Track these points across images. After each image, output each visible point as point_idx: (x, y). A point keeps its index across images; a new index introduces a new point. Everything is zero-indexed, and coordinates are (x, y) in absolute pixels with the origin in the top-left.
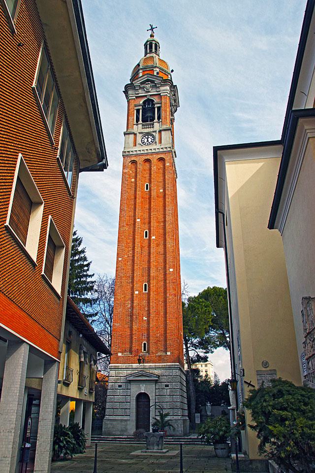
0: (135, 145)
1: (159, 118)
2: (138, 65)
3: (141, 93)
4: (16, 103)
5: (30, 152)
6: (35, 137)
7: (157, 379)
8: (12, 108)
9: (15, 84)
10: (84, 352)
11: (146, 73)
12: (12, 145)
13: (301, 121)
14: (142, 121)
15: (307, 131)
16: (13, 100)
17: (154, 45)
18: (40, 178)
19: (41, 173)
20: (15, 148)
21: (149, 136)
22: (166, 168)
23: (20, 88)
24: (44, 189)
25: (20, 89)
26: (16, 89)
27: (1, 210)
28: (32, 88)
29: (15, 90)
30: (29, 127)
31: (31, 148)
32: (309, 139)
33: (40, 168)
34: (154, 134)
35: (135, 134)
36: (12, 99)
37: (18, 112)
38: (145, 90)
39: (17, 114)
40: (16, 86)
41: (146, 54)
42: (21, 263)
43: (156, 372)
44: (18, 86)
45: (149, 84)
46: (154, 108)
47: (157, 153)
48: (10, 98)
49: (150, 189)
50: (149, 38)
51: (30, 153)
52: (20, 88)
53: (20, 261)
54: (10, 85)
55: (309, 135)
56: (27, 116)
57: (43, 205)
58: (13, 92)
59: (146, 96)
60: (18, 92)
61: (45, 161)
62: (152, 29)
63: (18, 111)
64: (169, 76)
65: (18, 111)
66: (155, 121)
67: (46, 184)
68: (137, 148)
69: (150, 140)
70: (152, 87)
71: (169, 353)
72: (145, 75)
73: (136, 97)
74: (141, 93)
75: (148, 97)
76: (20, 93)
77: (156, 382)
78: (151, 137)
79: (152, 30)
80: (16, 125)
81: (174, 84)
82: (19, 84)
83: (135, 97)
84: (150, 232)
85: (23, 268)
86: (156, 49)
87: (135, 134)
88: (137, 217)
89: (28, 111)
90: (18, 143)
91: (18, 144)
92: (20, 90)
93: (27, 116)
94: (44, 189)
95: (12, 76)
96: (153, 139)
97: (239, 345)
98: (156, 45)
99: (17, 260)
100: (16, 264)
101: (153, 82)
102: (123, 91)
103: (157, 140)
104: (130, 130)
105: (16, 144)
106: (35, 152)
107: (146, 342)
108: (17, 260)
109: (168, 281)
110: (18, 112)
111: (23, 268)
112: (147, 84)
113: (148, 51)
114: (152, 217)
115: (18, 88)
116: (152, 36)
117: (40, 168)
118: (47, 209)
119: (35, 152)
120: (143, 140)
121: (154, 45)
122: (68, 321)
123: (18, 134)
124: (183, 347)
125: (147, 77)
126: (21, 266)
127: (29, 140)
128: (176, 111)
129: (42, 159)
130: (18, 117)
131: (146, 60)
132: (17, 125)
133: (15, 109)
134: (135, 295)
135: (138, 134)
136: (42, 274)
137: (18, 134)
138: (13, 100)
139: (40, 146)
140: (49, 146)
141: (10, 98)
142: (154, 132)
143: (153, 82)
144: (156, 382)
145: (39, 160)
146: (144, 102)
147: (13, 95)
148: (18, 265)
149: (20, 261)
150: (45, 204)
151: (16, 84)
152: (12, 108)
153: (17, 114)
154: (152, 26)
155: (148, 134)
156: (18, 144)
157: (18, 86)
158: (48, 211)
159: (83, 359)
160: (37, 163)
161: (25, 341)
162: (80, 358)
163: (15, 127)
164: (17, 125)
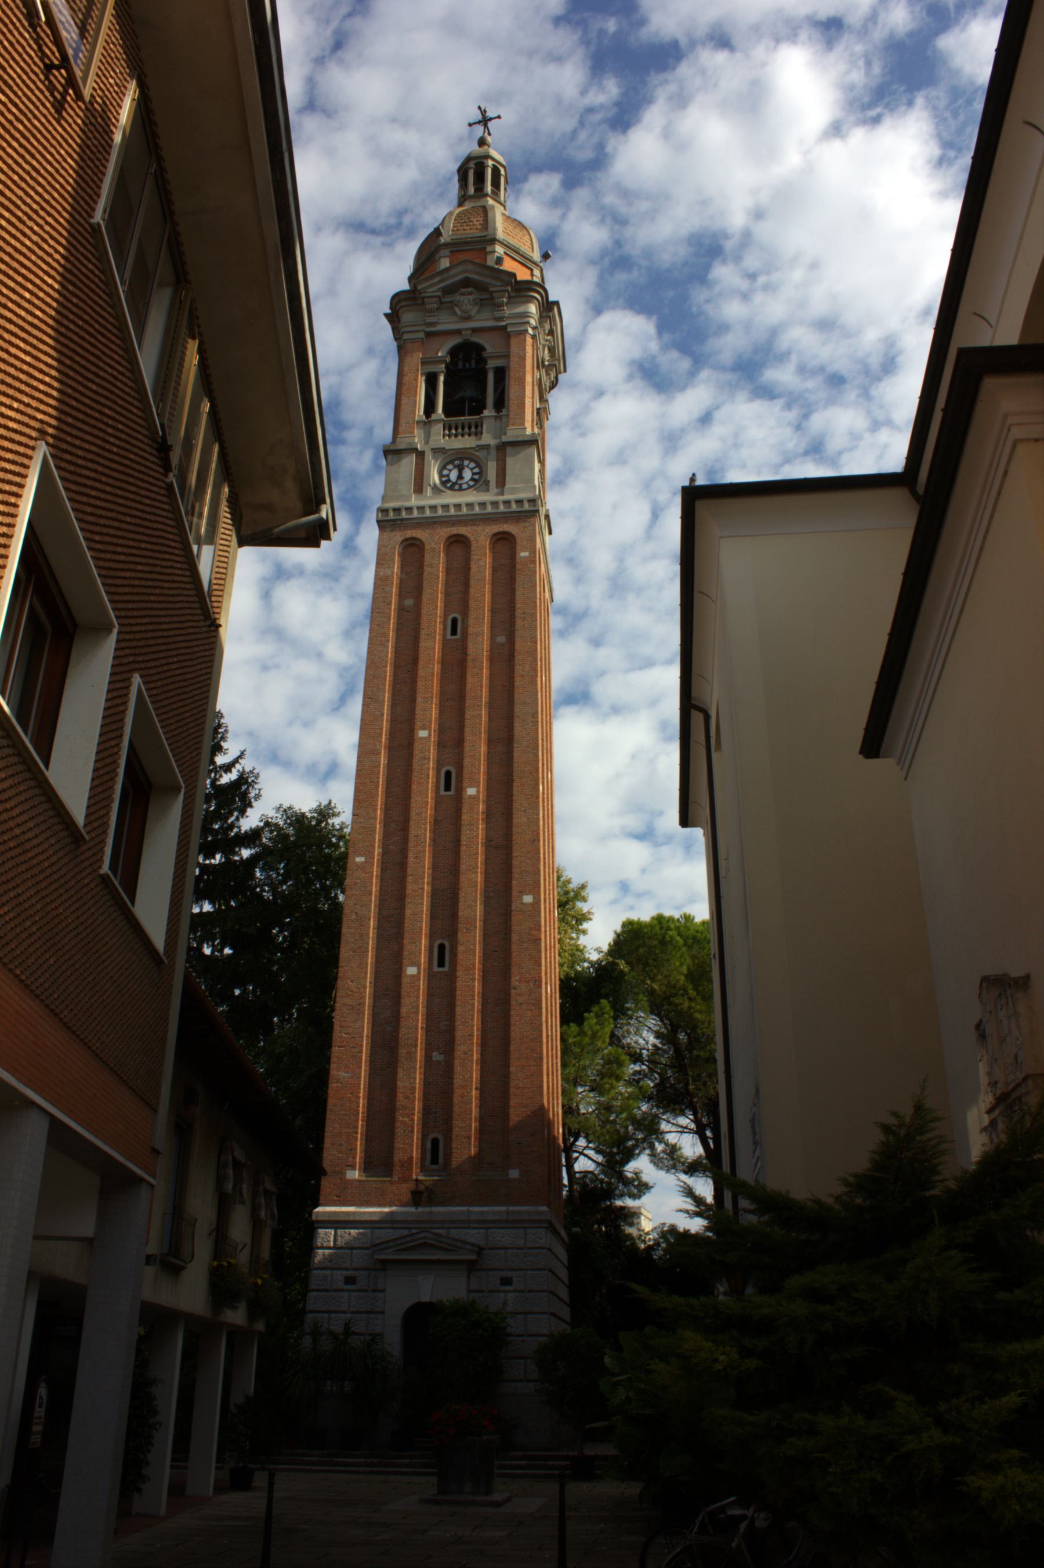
0: (419, 489)
2: (437, 233)
3: (446, 322)
4: (35, 264)
5: (77, 442)
6: (94, 396)
7: (473, 1257)
8: (20, 279)
9: (31, 197)
10: (236, 1164)
11: (462, 257)
12: (16, 405)
13: (990, 384)
14: (445, 411)
15: (1010, 421)
16: (24, 250)
17: (489, 172)
18: (108, 539)
19: (112, 523)
20: (26, 420)
21: (466, 463)
22: (518, 566)
23: (49, 214)
24: (119, 582)
25: (50, 220)
26: (35, 216)
27: (2, 848)
28: (91, 225)
29: (30, 218)
30: (77, 358)
31: (80, 429)
32: (1015, 443)
33: (109, 505)
34: (481, 454)
35: (421, 455)
36: (18, 245)
37: (38, 298)
38: (455, 314)
39: (36, 301)
40: (35, 206)
41: (462, 200)
42: (31, 824)
43: (474, 1236)
44: (42, 208)
45: (470, 293)
46: (484, 373)
47: (486, 519)
48: (13, 242)
50: (474, 148)
51: (74, 446)
52: (49, 214)
53: (25, 817)
54: (14, 198)
55: (1016, 433)
56: (71, 317)
57: (114, 636)
58: (24, 223)
59: (458, 332)
60: (41, 227)
61: (125, 486)
62: (485, 121)
63: (41, 294)
64: (537, 272)
65: (41, 294)
66: (486, 413)
67: (127, 566)
68: (429, 499)
69: (467, 474)
70: (482, 303)
71: (514, 1174)
72: (458, 264)
73: (429, 335)
74: (446, 322)
75: (467, 335)
76: (48, 233)
77: (471, 1267)
78: (472, 465)
79: (486, 126)
80: (37, 394)
81: (551, 298)
82: (47, 202)
83: (422, 335)
85: (35, 842)
86: (496, 184)
87: (421, 455)
88: (418, 724)
89: (75, 300)
90: (34, 403)
91: (37, 410)
92: (47, 223)
93: (71, 317)
94: (119, 582)
95: (23, 169)
96: (477, 470)
97: (755, 1143)
99: (17, 811)
100: (12, 824)
101: (480, 287)
102: (386, 315)
104: (401, 445)
105: (28, 405)
106: (93, 448)
108: (17, 811)
109: (515, 937)
110: (38, 298)
111: (35, 842)
112: (463, 294)
113: (471, 190)
115: (42, 213)
116: (482, 142)
117: (109, 505)
118: (127, 651)
119: (93, 448)
120: (445, 472)
121: (489, 172)
122: (252, 795)
123: (36, 374)
124: (560, 1160)
125: (466, 271)
126: (30, 835)
127: (74, 403)
128: (554, 385)
129: (116, 475)
130: (38, 313)
131: (462, 219)
132: (35, 342)
133: (30, 286)
134: (405, 981)
135: (429, 456)
136: (102, 872)
137: (36, 374)
138: (24, 250)
139: (110, 430)
140: (140, 437)
141: (13, 242)
142: (481, 447)
143: (480, 287)
144: (471, 1267)
145: (104, 479)
146: (453, 352)
147: (25, 235)
148: (17, 831)
149: (25, 817)
150: (119, 633)
151: (37, 198)
152: (20, 279)
153: (36, 301)
154: (483, 112)
156: (37, 410)
157: (42, 208)
158: (131, 659)
159: (229, 1186)
160: (97, 485)
161: (33, 1103)
162: (220, 1181)
163: (28, 348)
164: (35, 342)
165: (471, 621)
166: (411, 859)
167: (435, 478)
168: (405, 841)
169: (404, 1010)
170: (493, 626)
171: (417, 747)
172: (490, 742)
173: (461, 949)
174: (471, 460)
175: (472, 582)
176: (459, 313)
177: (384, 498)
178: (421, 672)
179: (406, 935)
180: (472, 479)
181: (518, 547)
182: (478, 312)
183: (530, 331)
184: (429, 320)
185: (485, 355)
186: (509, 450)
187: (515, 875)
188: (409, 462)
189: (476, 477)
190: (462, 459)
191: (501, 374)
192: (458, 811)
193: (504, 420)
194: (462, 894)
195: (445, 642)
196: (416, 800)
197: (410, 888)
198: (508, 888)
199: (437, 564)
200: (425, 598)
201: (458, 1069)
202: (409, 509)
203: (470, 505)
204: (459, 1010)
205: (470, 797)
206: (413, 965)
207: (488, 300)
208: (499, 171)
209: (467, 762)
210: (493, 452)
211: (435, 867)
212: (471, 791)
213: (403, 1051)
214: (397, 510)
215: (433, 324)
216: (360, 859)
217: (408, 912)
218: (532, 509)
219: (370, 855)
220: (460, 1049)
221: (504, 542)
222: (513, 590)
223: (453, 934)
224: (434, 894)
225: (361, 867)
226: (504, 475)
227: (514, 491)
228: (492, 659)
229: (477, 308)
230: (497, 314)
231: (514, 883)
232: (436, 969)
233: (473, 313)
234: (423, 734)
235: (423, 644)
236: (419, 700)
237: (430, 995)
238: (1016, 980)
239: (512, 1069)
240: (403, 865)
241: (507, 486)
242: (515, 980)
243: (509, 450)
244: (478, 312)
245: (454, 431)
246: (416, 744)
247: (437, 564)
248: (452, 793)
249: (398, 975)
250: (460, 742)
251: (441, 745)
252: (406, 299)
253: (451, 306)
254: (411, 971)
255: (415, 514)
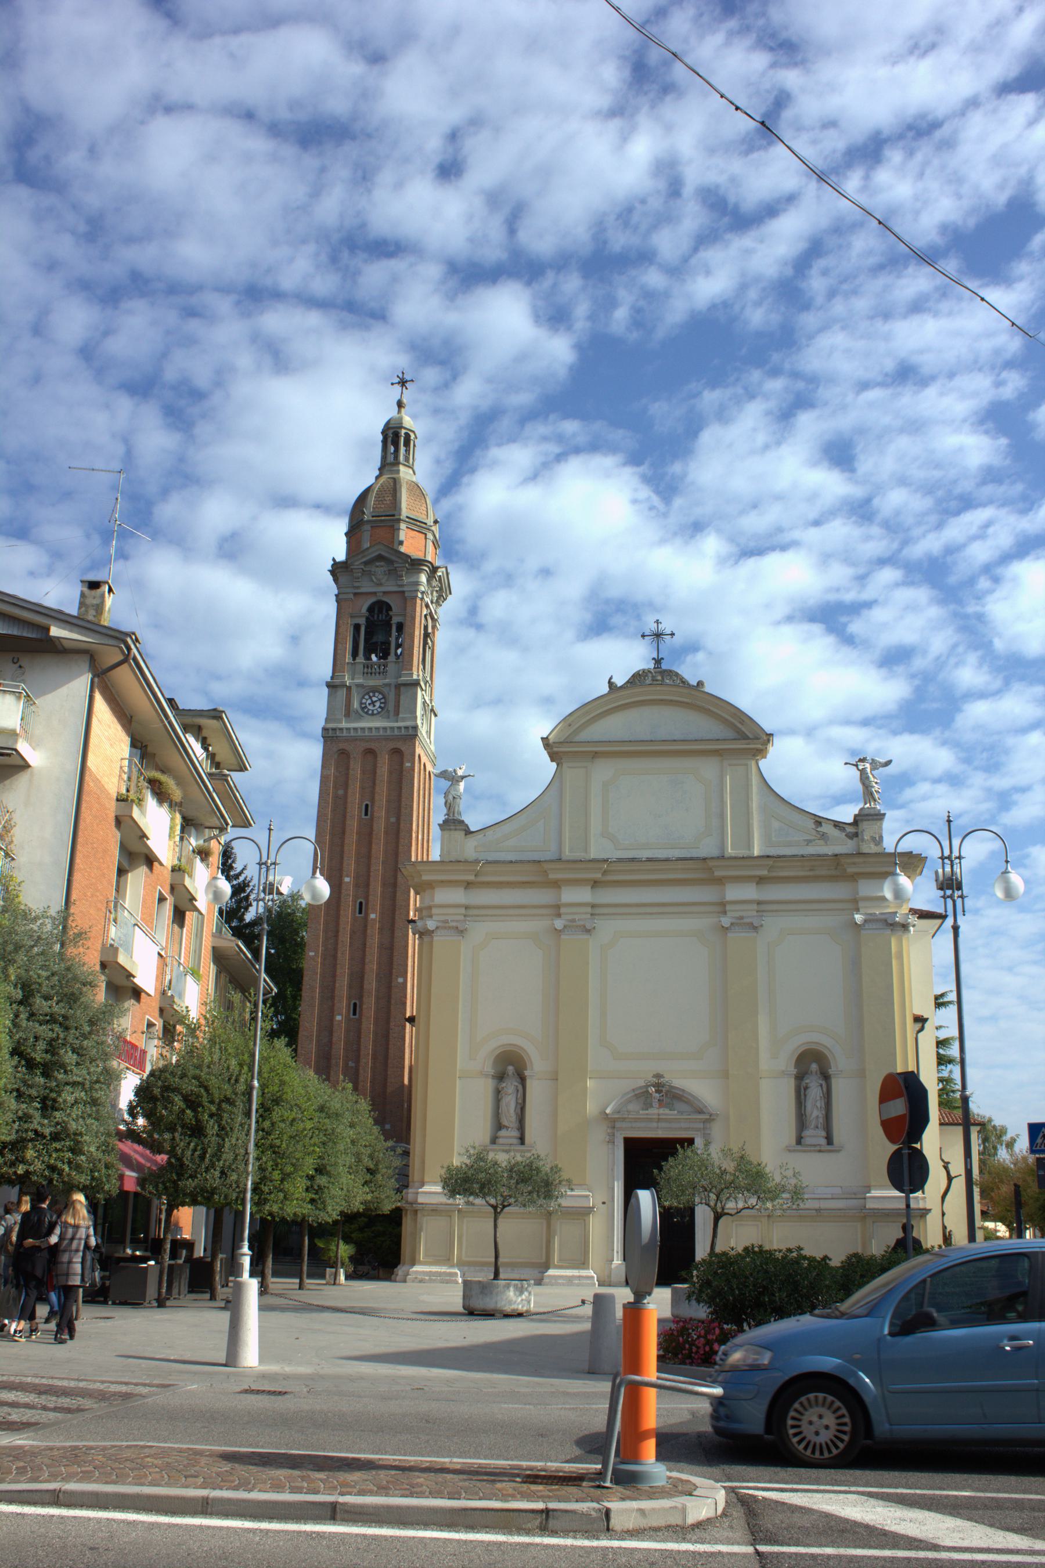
1: (393, 515)
34: (385, 690)
46: (390, 626)
47: (387, 739)
49: (372, 815)
59: (375, 593)
73: (355, 594)
74: (366, 587)
83: (351, 596)
84: (367, 904)
98: (407, 436)
103: (391, 706)
104: (337, 681)
107: (362, 900)
109: (393, 1002)
114: (372, 874)
120: (364, 701)
134: (335, 1023)
142: (386, 685)
146: (371, 609)
155: (374, 690)
165: (376, 808)
166: (339, 955)
167: (356, 705)
168: (336, 943)
169: (334, 1039)
170: (388, 812)
171: (344, 887)
172: (384, 885)
173: (364, 1006)
174: (380, 693)
175: (377, 782)
176: (375, 580)
177: (327, 720)
178: (346, 841)
179: (336, 998)
180: (380, 707)
181: (405, 760)
182: (387, 580)
183: (420, 595)
184: (356, 584)
185: (391, 613)
186: (402, 688)
187: (395, 967)
188: (342, 693)
189: (382, 705)
190: (374, 692)
191: (400, 627)
192: (366, 926)
193: (401, 664)
194: (366, 976)
195: (360, 819)
196: (342, 920)
197: (339, 971)
198: (391, 973)
199: (356, 770)
200: (350, 791)
201: (361, 1071)
202: (341, 729)
203: (377, 729)
204: (369, 931)
205: (372, 919)
206: (339, 1014)
207: (394, 573)
208: (410, 436)
209: (371, 898)
210: (393, 689)
211: (351, 959)
212: (373, 916)
213: (333, 1061)
214: (334, 729)
215: (358, 587)
216: (312, 954)
217: (337, 985)
218: (413, 733)
219: (317, 952)
220: (363, 1061)
221: (397, 753)
222: (401, 788)
223: (361, 997)
224: (351, 975)
225: (313, 958)
226: (399, 706)
227: (404, 720)
228: (386, 833)
229: (386, 577)
230: (400, 583)
231: (394, 971)
232: (352, 1016)
233: (383, 581)
234: (347, 880)
235: (348, 822)
236: (345, 858)
237: (347, 1031)
238: (449, 809)
239: (389, 1073)
240: (335, 957)
241: (400, 716)
242: (392, 1024)
243: (402, 688)
244: (387, 580)
245: (370, 670)
246: (343, 885)
247: (356, 770)
248: (362, 915)
249: (332, 1019)
250: (367, 885)
251: (357, 885)
252: (341, 567)
253: (370, 573)
254: (338, 1018)
255: (345, 734)
